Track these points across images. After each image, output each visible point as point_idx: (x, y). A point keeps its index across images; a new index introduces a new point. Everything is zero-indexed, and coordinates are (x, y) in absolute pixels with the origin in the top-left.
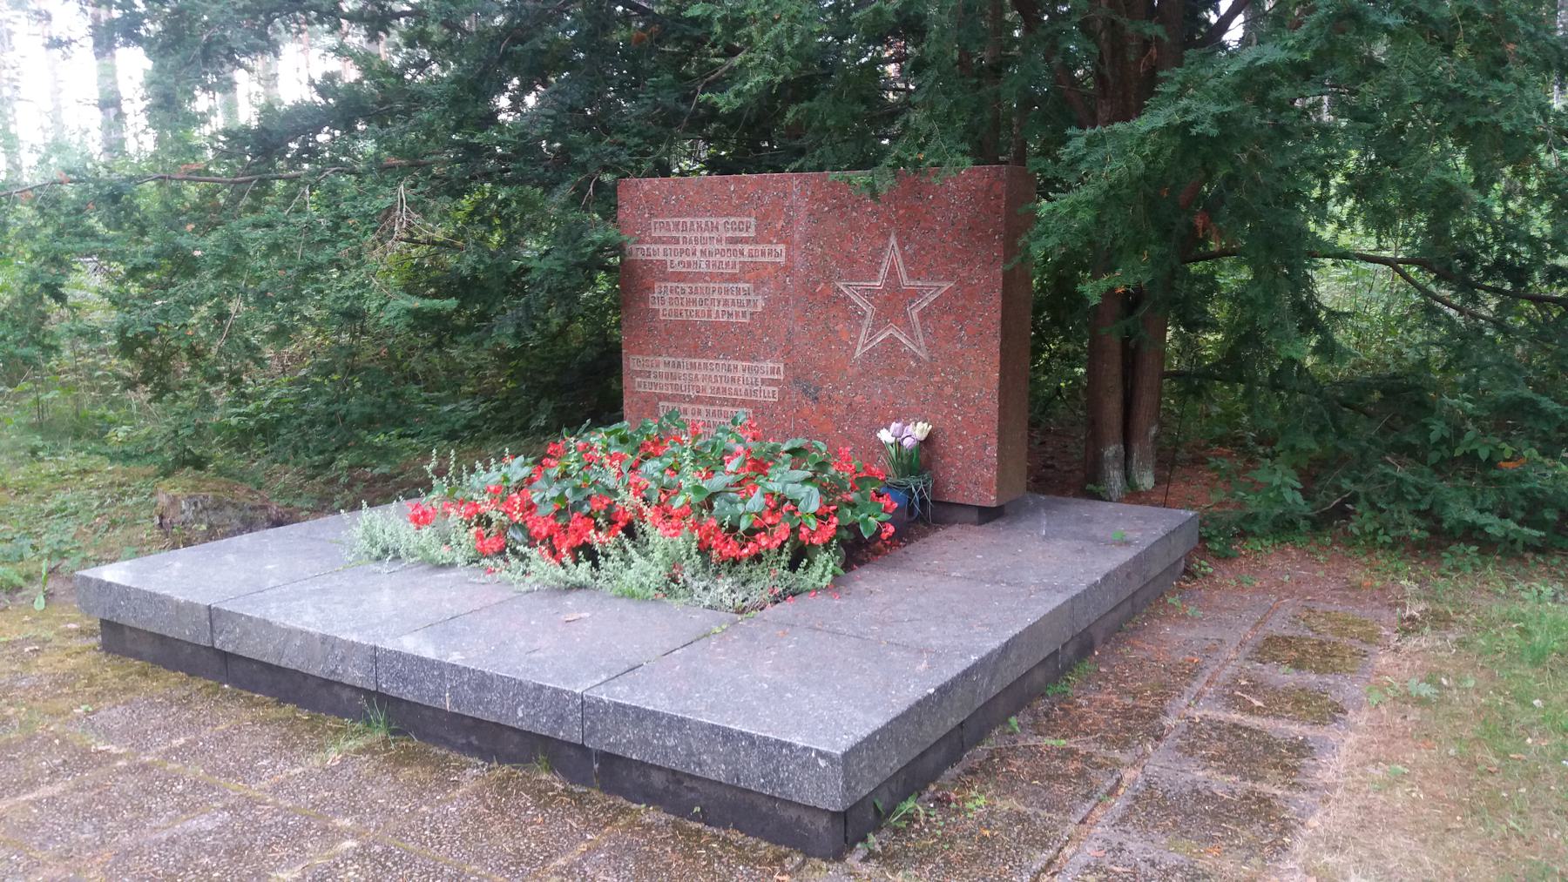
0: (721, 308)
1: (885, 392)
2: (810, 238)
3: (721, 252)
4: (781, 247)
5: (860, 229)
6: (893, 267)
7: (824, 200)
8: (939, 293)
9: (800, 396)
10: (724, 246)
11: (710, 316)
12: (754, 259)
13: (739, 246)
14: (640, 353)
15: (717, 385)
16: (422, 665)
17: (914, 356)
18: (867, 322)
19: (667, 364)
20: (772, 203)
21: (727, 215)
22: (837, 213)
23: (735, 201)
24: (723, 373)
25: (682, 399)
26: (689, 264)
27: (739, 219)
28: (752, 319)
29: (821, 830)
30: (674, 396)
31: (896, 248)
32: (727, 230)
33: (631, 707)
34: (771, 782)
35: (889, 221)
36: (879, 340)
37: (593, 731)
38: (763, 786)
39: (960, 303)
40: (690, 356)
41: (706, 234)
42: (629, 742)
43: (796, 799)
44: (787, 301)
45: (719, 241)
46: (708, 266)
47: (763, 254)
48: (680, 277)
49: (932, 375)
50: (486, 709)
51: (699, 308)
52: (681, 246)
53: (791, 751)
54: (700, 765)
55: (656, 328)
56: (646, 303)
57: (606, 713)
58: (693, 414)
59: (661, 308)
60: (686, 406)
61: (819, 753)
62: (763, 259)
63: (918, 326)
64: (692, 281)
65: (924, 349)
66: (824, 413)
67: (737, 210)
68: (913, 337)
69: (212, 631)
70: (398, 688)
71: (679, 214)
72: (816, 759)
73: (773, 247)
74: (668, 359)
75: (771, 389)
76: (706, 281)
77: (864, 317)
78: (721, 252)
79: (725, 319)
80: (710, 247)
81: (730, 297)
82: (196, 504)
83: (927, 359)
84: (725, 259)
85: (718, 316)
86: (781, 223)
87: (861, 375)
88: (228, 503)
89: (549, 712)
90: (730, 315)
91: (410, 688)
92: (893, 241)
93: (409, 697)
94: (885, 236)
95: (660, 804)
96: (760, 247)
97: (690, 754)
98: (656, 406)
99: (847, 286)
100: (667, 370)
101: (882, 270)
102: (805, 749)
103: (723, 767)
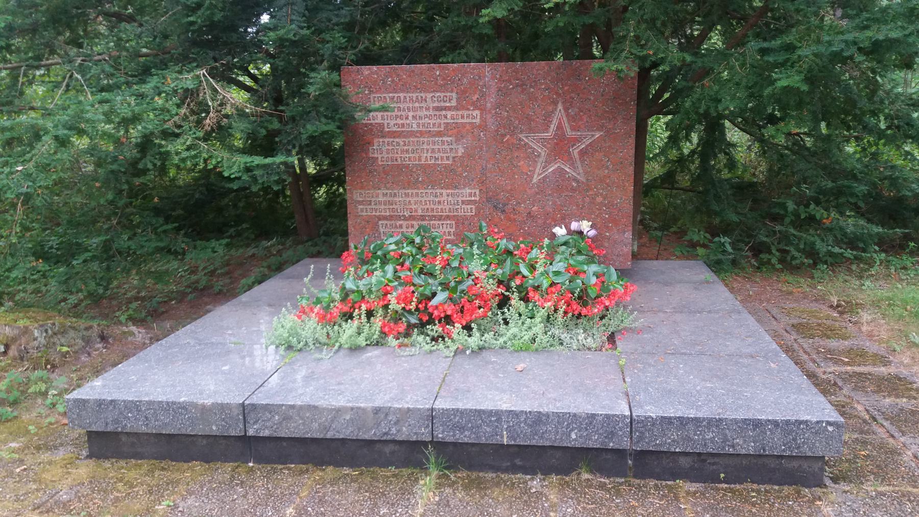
0: (429, 154)
1: (554, 203)
2: (498, 105)
3: (429, 117)
4: (477, 113)
5: (536, 99)
6: (560, 123)
7: (509, 81)
8: (593, 139)
9: (492, 210)
10: (431, 112)
11: (420, 160)
12: (456, 121)
13: (444, 112)
14: (362, 188)
15: (426, 207)
16: (480, 415)
17: (575, 180)
18: (542, 159)
19: (385, 195)
20: (470, 83)
21: (434, 91)
22: (519, 89)
23: (440, 82)
24: (432, 198)
25: (399, 218)
26: (403, 125)
27: (443, 94)
28: (454, 161)
29: (816, 470)
30: (391, 216)
31: (562, 111)
32: (434, 102)
33: (675, 418)
34: (789, 448)
35: (557, 93)
36: (550, 170)
37: (641, 438)
38: (784, 450)
39: (607, 145)
40: (404, 188)
41: (417, 105)
42: (673, 441)
43: (810, 454)
44: (481, 149)
45: (427, 109)
46: (418, 126)
47: (463, 117)
48: (394, 134)
49: (588, 191)
50: (542, 437)
51: (411, 155)
52: (396, 113)
53: (807, 426)
54: (733, 446)
55: (376, 170)
56: (367, 154)
57: (653, 425)
58: (407, 228)
59: (380, 156)
60: (401, 222)
61: (829, 423)
62: (463, 121)
63: (578, 160)
64: (405, 137)
65: (582, 175)
66: (509, 219)
67: (443, 88)
68: (574, 168)
69: (245, 421)
70: (454, 435)
71: (395, 91)
72: (826, 427)
73: (470, 112)
74: (385, 192)
75: (469, 207)
76: (417, 137)
77: (539, 156)
78: (429, 117)
79: (433, 162)
80: (419, 113)
81: (436, 147)
82: (46, 331)
83: (585, 181)
84: (432, 122)
85: (426, 160)
86: (477, 96)
87: (537, 193)
88: (70, 327)
89: (601, 431)
90: (437, 159)
91: (467, 433)
92: (560, 107)
93: (466, 440)
94: (555, 103)
95: (687, 478)
96: (460, 113)
97: (725, 440)
98: (377, 224)
99: (527, 137)
100: (385, 199)
101: (552, 126)
102: (818, 422)
103: (753, 444)
